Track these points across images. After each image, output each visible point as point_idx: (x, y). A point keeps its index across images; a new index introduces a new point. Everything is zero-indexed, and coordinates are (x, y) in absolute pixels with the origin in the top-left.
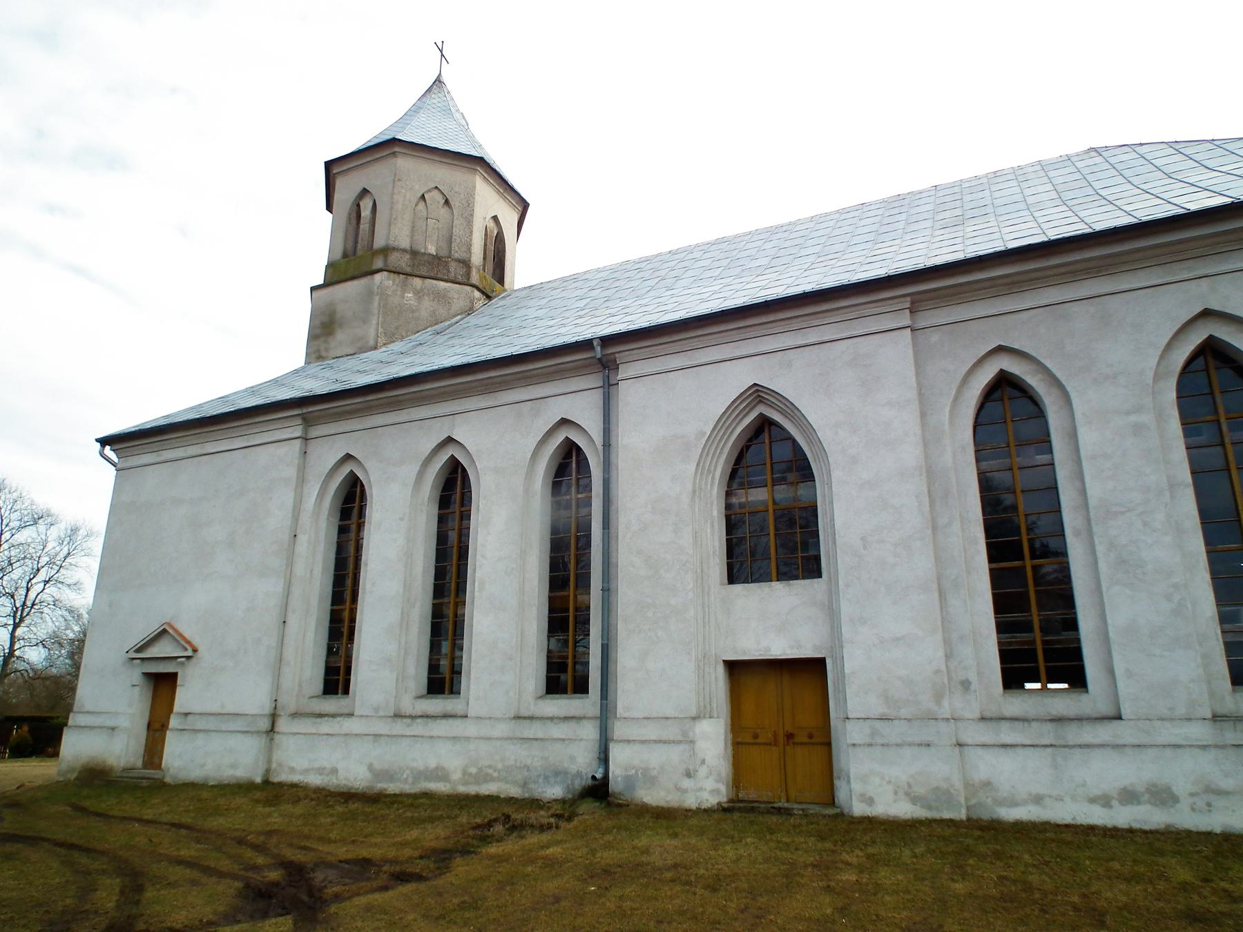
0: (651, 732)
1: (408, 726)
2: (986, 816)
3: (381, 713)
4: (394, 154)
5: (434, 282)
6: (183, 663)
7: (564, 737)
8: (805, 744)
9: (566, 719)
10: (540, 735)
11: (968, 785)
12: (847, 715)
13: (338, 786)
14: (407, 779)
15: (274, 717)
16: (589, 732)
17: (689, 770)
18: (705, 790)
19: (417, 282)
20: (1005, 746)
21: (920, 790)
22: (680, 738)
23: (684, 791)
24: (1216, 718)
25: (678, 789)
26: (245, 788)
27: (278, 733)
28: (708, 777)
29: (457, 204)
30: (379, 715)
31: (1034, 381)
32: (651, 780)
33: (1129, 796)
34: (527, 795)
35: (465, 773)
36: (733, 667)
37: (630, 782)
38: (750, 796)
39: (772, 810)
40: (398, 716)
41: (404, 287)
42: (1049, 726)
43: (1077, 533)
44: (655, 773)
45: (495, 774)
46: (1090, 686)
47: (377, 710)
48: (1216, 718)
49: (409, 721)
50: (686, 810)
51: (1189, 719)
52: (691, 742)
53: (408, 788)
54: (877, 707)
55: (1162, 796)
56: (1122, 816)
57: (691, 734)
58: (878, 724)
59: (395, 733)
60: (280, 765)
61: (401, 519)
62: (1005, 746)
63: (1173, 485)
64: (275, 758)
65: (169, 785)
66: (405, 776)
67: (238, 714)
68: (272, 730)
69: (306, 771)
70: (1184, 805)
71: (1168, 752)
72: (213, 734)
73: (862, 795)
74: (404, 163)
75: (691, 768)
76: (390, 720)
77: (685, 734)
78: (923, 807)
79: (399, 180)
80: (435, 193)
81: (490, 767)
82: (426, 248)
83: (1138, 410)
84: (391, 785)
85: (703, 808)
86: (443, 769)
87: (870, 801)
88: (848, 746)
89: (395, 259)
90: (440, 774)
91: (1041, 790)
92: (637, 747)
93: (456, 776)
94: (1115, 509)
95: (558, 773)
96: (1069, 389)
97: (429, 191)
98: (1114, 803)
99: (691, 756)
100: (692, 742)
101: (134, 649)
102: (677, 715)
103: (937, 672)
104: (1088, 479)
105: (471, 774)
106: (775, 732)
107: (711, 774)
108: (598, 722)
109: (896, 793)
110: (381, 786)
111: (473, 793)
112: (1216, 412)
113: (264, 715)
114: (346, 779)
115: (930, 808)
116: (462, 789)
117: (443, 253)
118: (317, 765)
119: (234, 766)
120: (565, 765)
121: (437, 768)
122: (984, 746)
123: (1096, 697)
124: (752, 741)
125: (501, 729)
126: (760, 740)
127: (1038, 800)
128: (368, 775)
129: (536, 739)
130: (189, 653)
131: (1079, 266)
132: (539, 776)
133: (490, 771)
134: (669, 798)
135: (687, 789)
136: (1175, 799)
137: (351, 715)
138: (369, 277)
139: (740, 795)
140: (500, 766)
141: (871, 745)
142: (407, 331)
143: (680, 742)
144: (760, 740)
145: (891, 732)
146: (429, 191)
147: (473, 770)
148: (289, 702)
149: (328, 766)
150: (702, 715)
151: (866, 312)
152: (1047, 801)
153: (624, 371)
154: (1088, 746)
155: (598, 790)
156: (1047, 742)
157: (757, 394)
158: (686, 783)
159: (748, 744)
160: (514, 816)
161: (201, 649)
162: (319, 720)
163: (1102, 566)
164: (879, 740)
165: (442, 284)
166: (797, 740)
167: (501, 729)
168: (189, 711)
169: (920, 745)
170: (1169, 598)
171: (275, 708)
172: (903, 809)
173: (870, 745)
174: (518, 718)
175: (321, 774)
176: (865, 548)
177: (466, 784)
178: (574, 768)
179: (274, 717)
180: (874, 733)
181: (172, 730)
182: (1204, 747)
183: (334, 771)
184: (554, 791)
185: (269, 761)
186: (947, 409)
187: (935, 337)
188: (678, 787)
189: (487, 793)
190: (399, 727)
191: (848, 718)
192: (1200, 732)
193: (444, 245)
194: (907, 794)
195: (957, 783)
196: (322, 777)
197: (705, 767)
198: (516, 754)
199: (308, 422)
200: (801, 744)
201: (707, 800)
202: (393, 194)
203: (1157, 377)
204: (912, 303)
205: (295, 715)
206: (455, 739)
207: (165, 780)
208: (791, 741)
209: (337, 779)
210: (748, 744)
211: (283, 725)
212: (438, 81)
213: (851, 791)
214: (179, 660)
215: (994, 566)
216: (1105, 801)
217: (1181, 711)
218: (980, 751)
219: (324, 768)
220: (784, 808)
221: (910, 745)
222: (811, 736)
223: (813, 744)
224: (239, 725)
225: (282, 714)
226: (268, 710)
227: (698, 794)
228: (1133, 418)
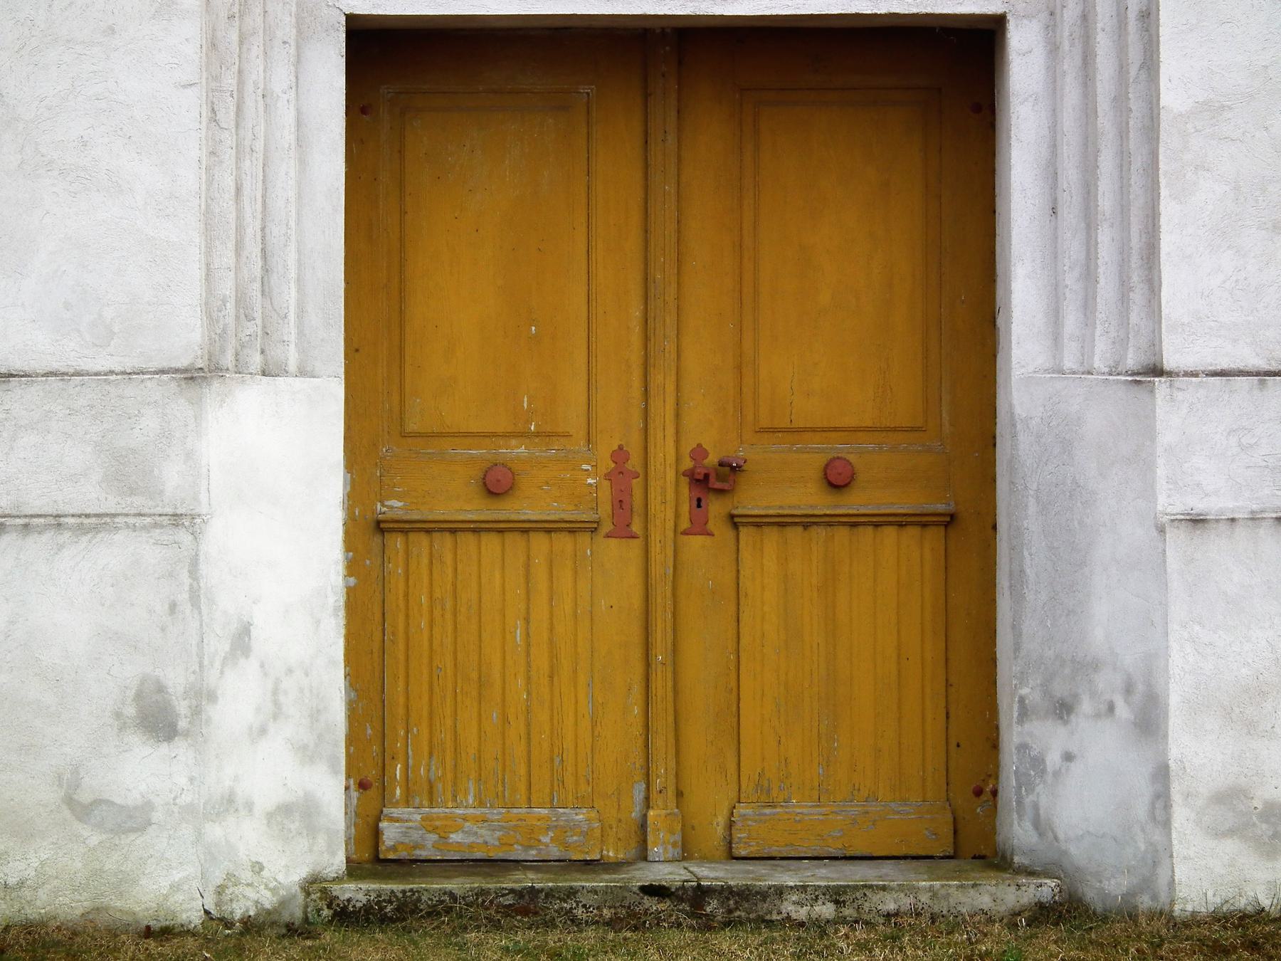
8: (807, 522)
12: (1155, 344)
17: (161, 689)
18: (249, 806)
28: (263, 731)
38: (455, 837)
39: (652, 904)
50: (148, 933)
52: (176, 519)
57: (172, 476)
75: (176, 679)
85: (238, 915)
88: (1161, 530)
99: (173, 607)
106: (620, 455)
107: (276, 715)
124: (475, 509)
126: (520, 508)
135: (148, 806)
139: (391, 833)
150: (228, 360)
160: (1000, 910)
188: (85, 797)
191: (1157, 371)
197: (250, 667)
200: (782, 522)
201: (258, 868)
208: (716, 508)
213: (1162, 774)
220: (726, 893)
223: (854, 523)
224: (266, 278)
227: (215, 832)
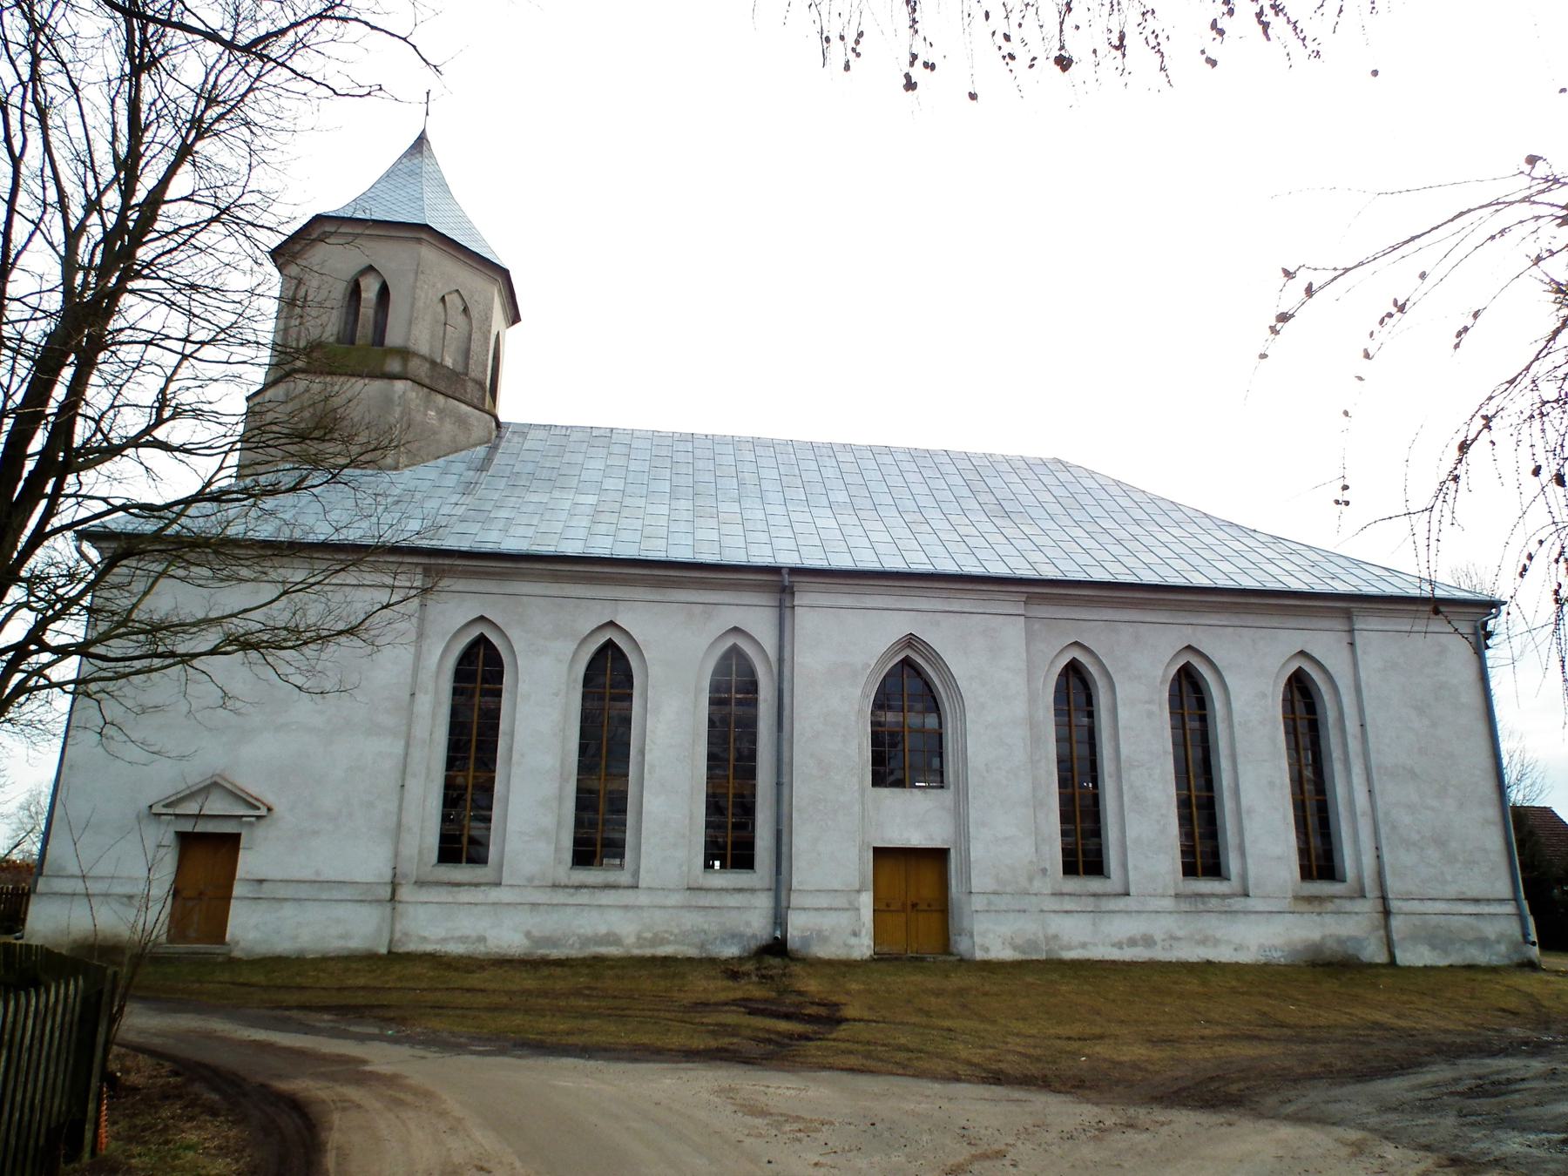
0: (823, 901)
1: (572, 895)
2: (1054, 956)
3: (536, 883)
4: (419, 240)
5: (456, 402)
6: (251, 824)
7: (739, 905)
9: (740, 890)
10: (716, 903)
11: (1046, 937)
13: (488, 954)
14: (573, 945)
15: (394, 885)
16: (764, 902)
19: (440, 399)
20: (1066, 912)
21: (1018, 941)
22: (847, 906)
23: (852, 947)
24: (1177, 896)
25: (846, 945)
26: (369, 959)
27: (400, 902)
29: (477, 316)
30: (534, 884)
31: (1093, 669)
32: (823, 938)
33: (1132, 942)
34: (704, 955)
35: (639, 937)
36: (877, 851)
37: (806, 940)
40: (555, 886)
41: (428, 403)
42: (1092, 899)
43: (1110, 776)
44: (827, 933)
45: (672, 938)
46: (1112, 875)
47: (531, 879)
48: (1177, 896)
49: (572, 890)
51: (1163, 896)
53: (574, 953)
54: (990, 884)
55: (1148, 941)
56: (1128, 954)
58: (992, 897)
59: (555, 902)
60: (406, 934)
61: (556, 695)
62: (1066, 912)
63: (1165, 752)
64: (398, 927)
65: (240, 960)
66: (571, 942)
67: (344, 882)
68: (393, 899)
69: (444, 940)
70: (1159, 947)
71: (1153, 915)
72: (307, 903)
73: (982, 946)
74: (429, 254)
76: (548, 889)
77: (850, 903)
78: (1020, 952)
79: (422, 273)
80: (455, 296)
81: (666, 932)
82: (442, 360)
83: (1150, 702)
84: (555, 951)
86: (615, 934)
87: (987, 950)
89: (419, 368)
90: (613, 939)
91: (1087, 940)
92: (812, 914)
93: (631, 940)
94: (1136, 764)
95: (735, 936)
96: (1114, 680)
97: (450, 293)
98: (1125, 946)
100: (858, 909)
101: (163, 803)
102: (844, 888)
103: (1031, 862)
104: (1121, 742)
105: (645, 939)
108: (771, 894)
109: (1003, 943)
110: (541, 952)
111: (649, 955)
112: (1182, 708)
113: (385, 883)
114: (497, 947)
115: (1024, 953)
116: (636, 952)
117: (460, 369)
118: (457, 934)
119: (345, 936)
120: (742, 929)
121: (608, 935)
122: (1055, 912)
123: (1114, 883)
125: (674, 899)
126: (892, 908)
127: (1084, 946)
128: (526, 942)
129: (713, 908)
130: (263, 812)
131: (1128, 600)
132: (716, 939)
133: (666, 935)
134: (838, 953)
136: (1155, 943)
137: (498, 884)
138: (386, 381)
140: (676, 931)
141: (1024, 911)
142: (428, 455)
143: (848, 909)
144: (892, 908)
145: (1002, 902)
146: (450, 293)
147: (648, 935)
148: (410, 868)
149: (474, 934)
151: (996, 597)
152: (1089, 947)
153: (799, 599)
154: (1113, 912)
155: (777, 948)
156: (1089, 909)
157: (911, 641)
158: (853, 941)
159: (883, 911)
161: (276, 809)
162: (456, 889)
163: (1126, 798)
164: (993, 908)
165: (464, 407)
166: (919, 908)
167: (674, 899)
168: (264, 878)
169: (1019, 911)
170: (1158, 822)
171: (395, 875)
172: (1008, 954)
173: (987, 911)
174: (689, 889)
175: (464, 943)
176: (987, 771)
177: (640, 947)
178: (749, 932)
179: (394, 885)
180: (989, 903)
181: (237, 898)
182: (1170, 912)
183: (482, 939)
184: (731, 951)
185: (392, 932)
186: (1042, 680)
187: (1037, 626)
189: (663, 954)
190: (560, 897)
192: (1168, 903)
193: (460, 359)
194: (1010, 944)
195: (1041, 935)
196: (466, 946)
198: (691, 920)
199: (427, 571)
202: (414, 287)
203: (1162, 683)
204: (1027, 597)
205: (421, 883)
206: (626, 907)
207: (233, 955)
209: (486, 947)
210: (883, 911)
211: (405, 893)
212: (421, 142)
214: (244, 819)
215: (457, 685)
216: (1119, 945)
217: (1160, 891)
218: (1052, 915)
219: (467, 937)
221: (1013, 911)
222: (929, 905)
223: (931, 911)
224: (347, 893)
225: (403, 882)
226: (388, 878)
228: (1147, 706)
